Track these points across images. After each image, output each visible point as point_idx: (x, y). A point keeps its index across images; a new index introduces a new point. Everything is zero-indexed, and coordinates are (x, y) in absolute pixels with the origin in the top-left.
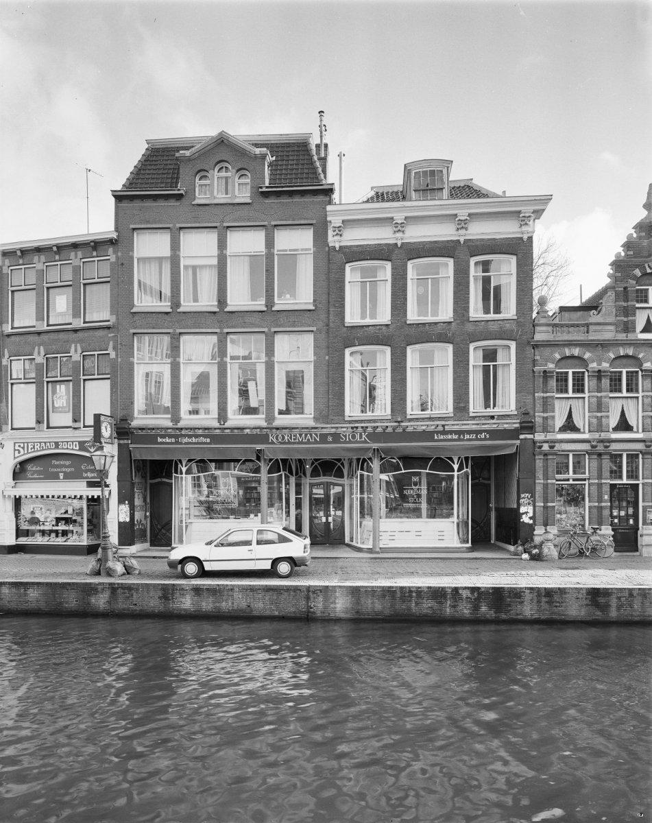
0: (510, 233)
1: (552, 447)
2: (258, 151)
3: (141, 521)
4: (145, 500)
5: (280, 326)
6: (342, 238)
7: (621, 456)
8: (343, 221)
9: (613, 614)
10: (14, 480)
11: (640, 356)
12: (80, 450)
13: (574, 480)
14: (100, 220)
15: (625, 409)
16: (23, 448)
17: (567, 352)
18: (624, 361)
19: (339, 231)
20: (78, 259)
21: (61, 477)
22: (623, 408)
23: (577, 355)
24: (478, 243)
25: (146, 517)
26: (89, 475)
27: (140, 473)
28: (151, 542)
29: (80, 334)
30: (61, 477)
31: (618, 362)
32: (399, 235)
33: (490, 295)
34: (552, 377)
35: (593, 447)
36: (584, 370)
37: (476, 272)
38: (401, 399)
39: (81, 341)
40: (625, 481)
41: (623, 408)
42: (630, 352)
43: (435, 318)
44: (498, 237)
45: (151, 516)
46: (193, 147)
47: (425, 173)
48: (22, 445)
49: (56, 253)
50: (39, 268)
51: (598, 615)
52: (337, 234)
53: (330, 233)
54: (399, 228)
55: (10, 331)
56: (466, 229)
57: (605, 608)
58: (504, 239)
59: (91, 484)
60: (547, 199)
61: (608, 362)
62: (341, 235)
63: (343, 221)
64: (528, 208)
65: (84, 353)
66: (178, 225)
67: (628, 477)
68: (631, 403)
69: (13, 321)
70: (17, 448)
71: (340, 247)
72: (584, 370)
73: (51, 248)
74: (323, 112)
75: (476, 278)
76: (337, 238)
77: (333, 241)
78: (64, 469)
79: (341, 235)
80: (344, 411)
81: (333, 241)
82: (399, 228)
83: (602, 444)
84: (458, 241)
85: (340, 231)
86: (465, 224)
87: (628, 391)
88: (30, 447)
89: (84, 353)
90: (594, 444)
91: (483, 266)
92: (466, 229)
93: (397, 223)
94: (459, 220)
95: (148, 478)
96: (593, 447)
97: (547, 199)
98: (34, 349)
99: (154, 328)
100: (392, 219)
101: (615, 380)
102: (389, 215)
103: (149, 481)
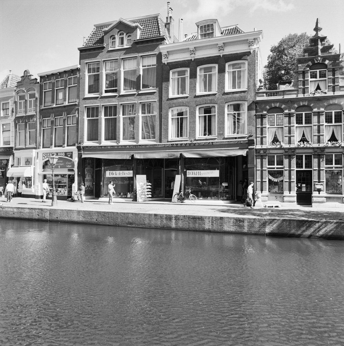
0: (244, 50)
1: (265, 152)
2: (134, 25)
3: (90, 186)
4: (92, 177)
5: (142, 100)
6: (224, 51)
7: (302, 156)
8: (195, 47)
9: (246, 230)
10: (43, 168)
11: (312, 105)
12: (65, 156)
13: (335, 168)
14: (72, 60)
15: (304, 132)
16: (46, 155)
17: (273, 105)
18: (304, 108)
19: (167, 56)
20: (66, 77)
21: (59, 167)
22: (303, 132)
23: (278, 106)
24: (179, 63)
25: (93, 185)
26: (69, 166)
27: (90, 166)
28: (95, 196)
29: (66, 108)
30: (59, 167)
31: (300, 109)
32: (193, 55)
33: (54, 99)
34: (323, 115)
35: (286, 152)
36: (311, 112)
37: (229, 69)
38: (193, 130)
39: (66, 111)
40: (304, 169)
41: (303, 132)
42: (306, 103)
43: (173, 96)
44: (238, 52)
45: (95, 184)
46: (112, 24)
47: (205, 26)
48: (45, 154)
49: (59, 75)
50: (53, 82)
51: (239, 230)
52: (165, 58)
53: (163, 57)
54: (192, 52)
55: (43, 108)
56: (223, 50)
57: (242, 227)
58: (241, 53)
59: (69, 170)
60: (260, 32)
61: (294, 109)
62: (167, 58)
63: (224, 43)
64: (221, 42)
65: (56, 117)
66: (103, 60)
67: (306, 167)
68: (308, 129)
69: (45, 103)
70: (44, 155)
71: (167, 63)
72: (311, 112)
73: (45, 76)
74: (169, 2)
75: (200, 76)
76: (166, 59)
77: (164, 61)
78: (60, 164)
79: (167, 58)
80: (168, 137)
81: (164, 61)
82: (192, 52)
83: (290, 150)
84: (220, 56)
85: (166, 56)
86: (222, 48)
87: (306, 123)
88: (48, 155)
89: (56, 117)
90: (287, 150)
91: (178, 73)
92: (223, 50)
93: (190, 50)
94: (219, 46)
95: (95, 168)
96: (286, 152)
97: (260, 32)
98: (50, 115)
99: (92, 104)
100: (189, 49)
101: (338, 116)
102: (246, 38)
103: (95, 169)
